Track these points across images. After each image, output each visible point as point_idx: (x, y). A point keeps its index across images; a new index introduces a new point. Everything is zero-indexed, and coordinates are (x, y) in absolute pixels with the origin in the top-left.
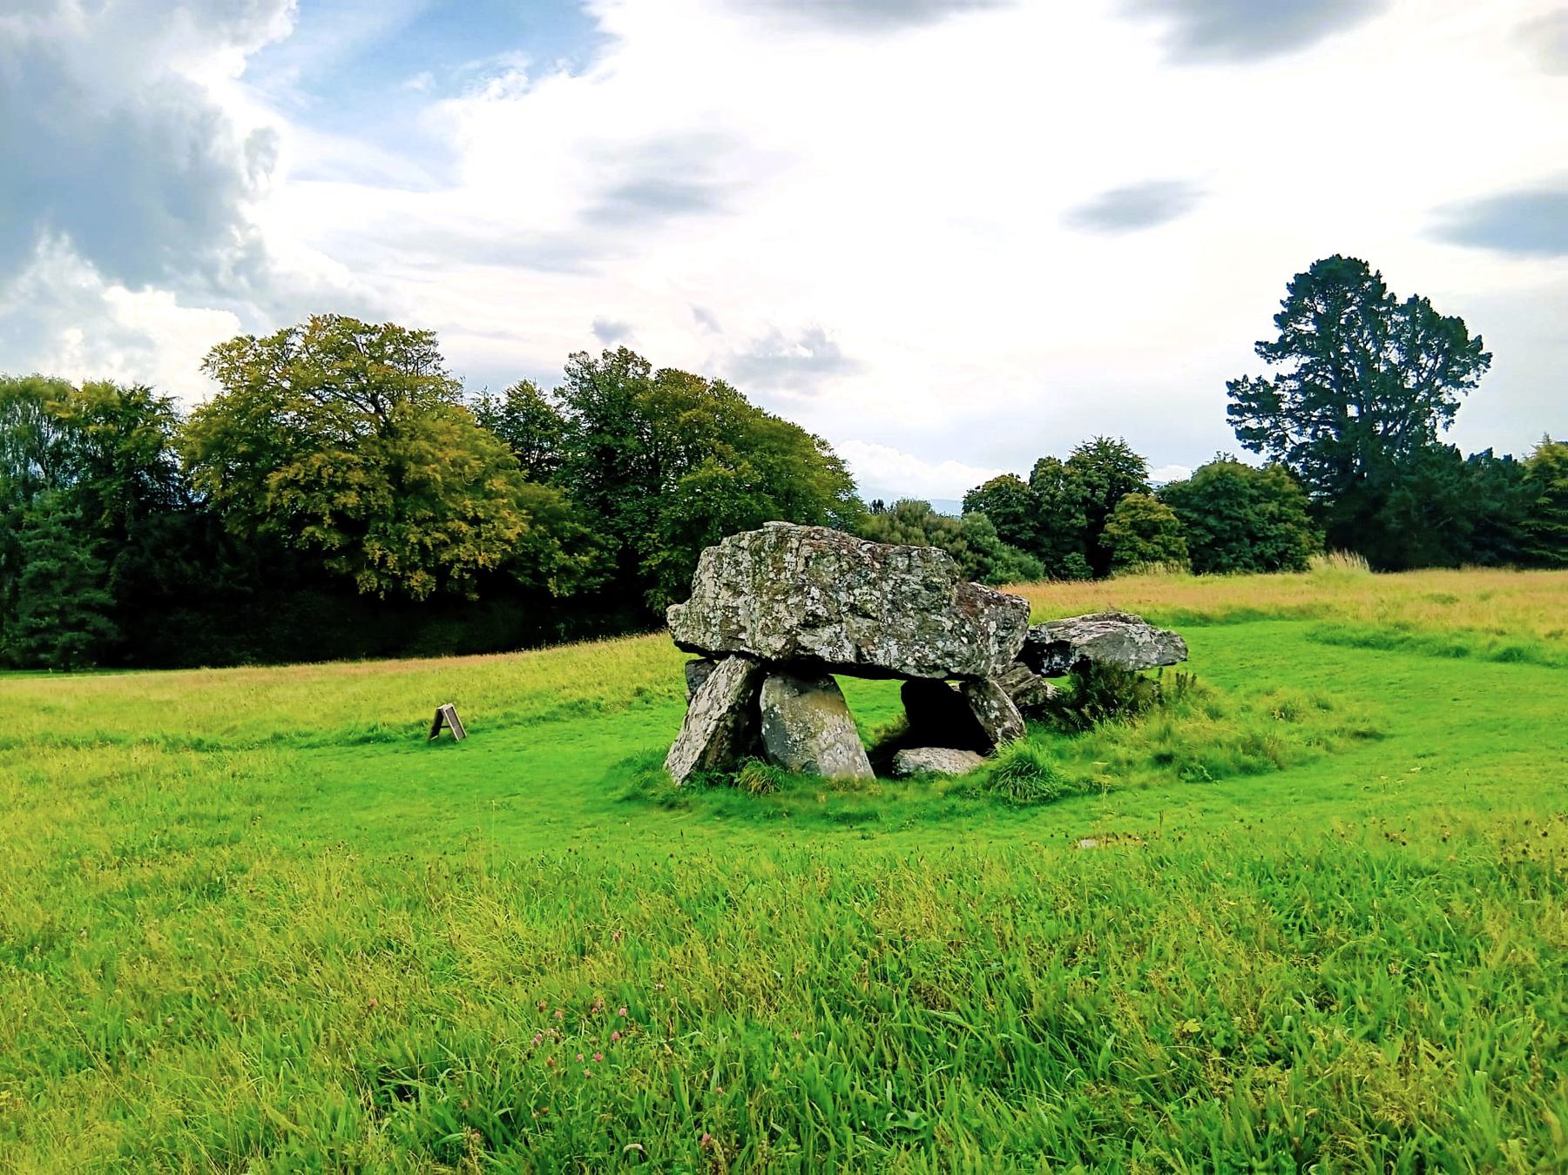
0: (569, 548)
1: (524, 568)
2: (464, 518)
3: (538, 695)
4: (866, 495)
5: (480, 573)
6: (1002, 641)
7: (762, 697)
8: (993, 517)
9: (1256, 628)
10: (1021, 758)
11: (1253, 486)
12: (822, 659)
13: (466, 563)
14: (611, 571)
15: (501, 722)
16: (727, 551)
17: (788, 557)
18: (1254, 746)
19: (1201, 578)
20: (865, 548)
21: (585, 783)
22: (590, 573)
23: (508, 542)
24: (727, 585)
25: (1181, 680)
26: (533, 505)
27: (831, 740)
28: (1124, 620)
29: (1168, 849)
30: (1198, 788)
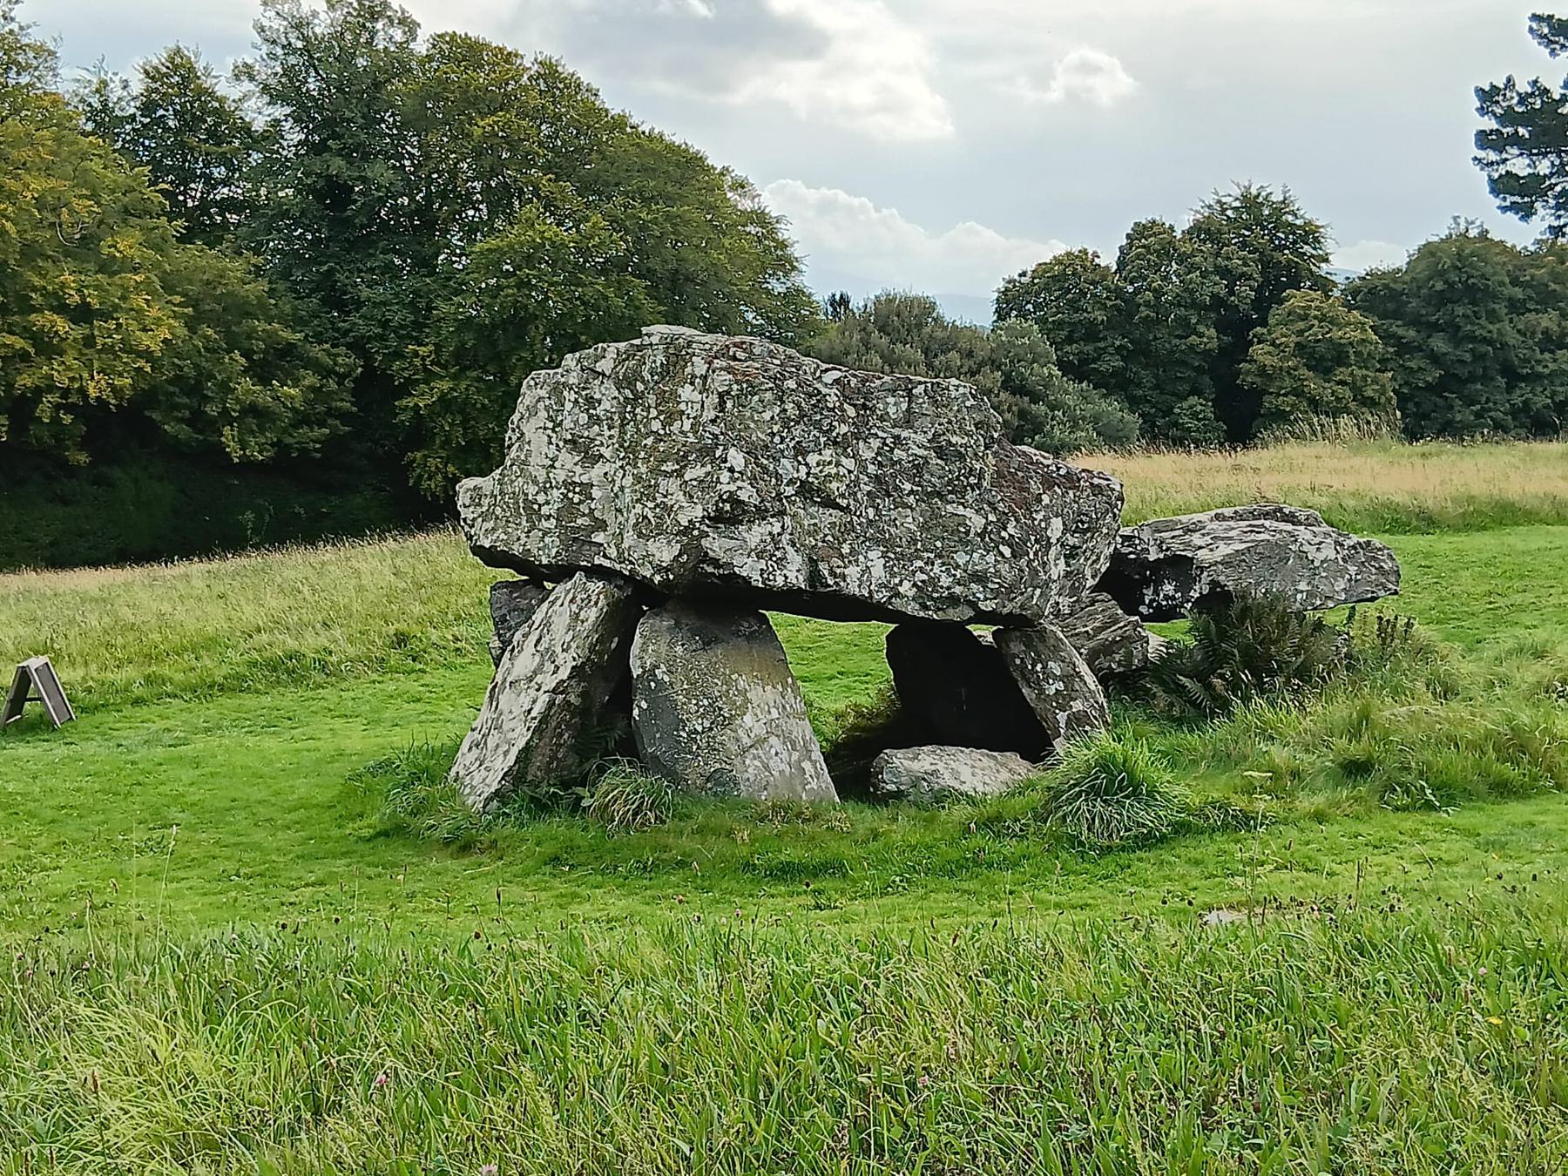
0: (262, 372)
1: (177, 407)
2: (62, 309)
3: (211, 643)
4: (818, 281)
5: (93, 414)
6: (1071, 554)
7: (635, 650)
8: (1048, 329)
9: (1521, 540)
10: (1105, 764)
11: (1515, 282)
12: (746, 581)
13: (66, 393)
14: (344, 416)
15: (137, 691)
16: (573, 380)
17: (686, 392)
18: (1516, 745)
19: (1419, 446)
20: (829, 377)
21: (302, 805)
22: (302, 419)
23: (147, 355)
24: (573, 442)
25: (1386, 629)
26: (193, 289)
27: (759, 730)
28: (1291, 519)
29: (1373, 924)
30: (1409, 822)
